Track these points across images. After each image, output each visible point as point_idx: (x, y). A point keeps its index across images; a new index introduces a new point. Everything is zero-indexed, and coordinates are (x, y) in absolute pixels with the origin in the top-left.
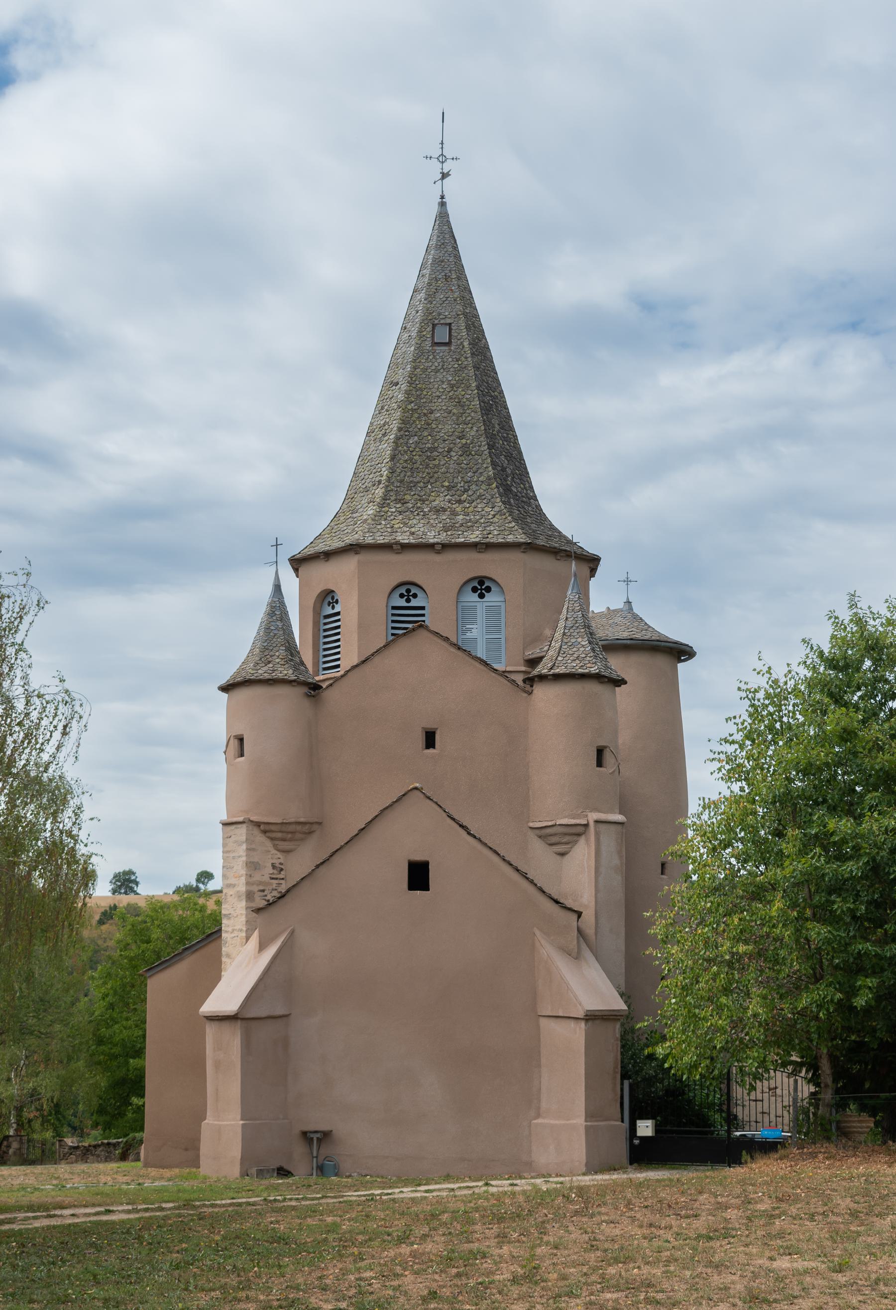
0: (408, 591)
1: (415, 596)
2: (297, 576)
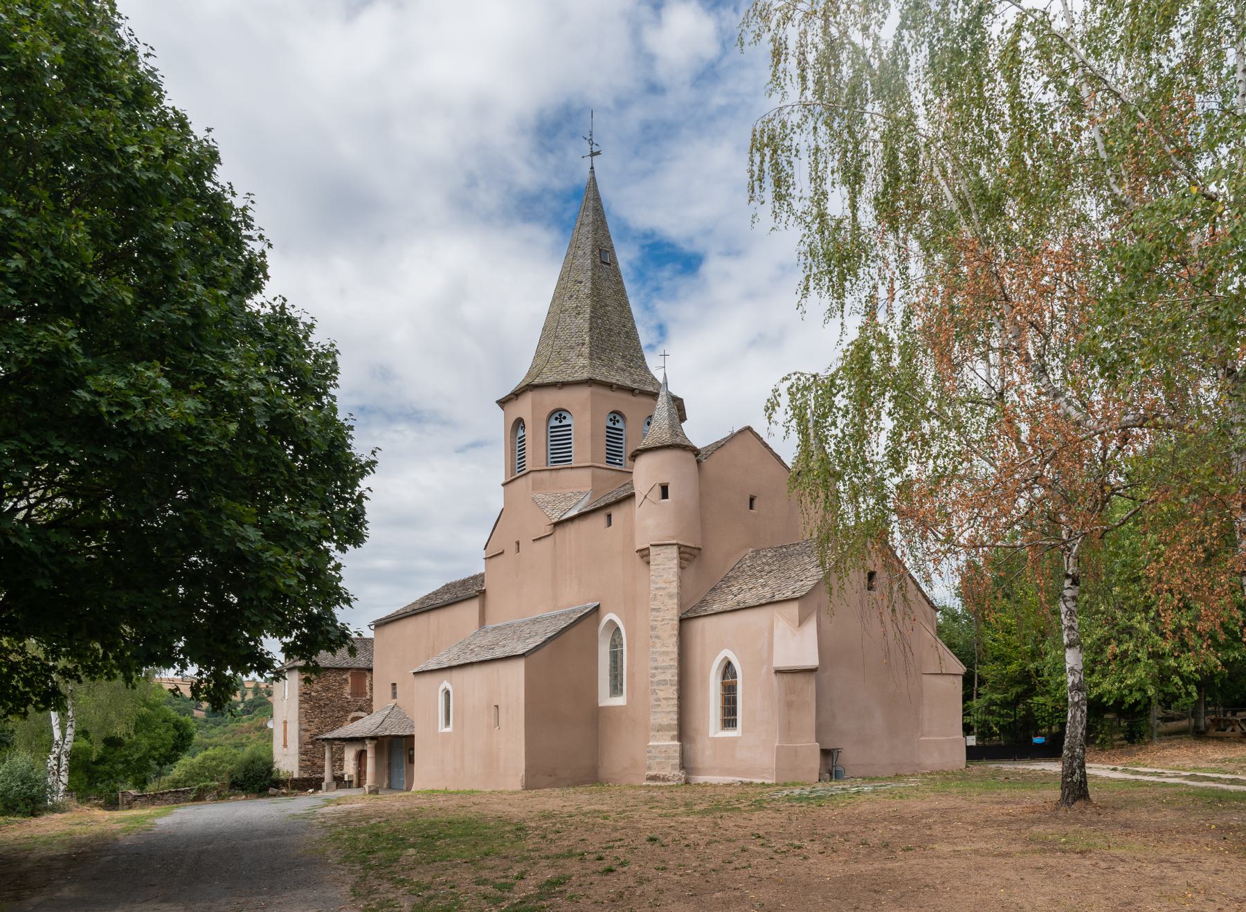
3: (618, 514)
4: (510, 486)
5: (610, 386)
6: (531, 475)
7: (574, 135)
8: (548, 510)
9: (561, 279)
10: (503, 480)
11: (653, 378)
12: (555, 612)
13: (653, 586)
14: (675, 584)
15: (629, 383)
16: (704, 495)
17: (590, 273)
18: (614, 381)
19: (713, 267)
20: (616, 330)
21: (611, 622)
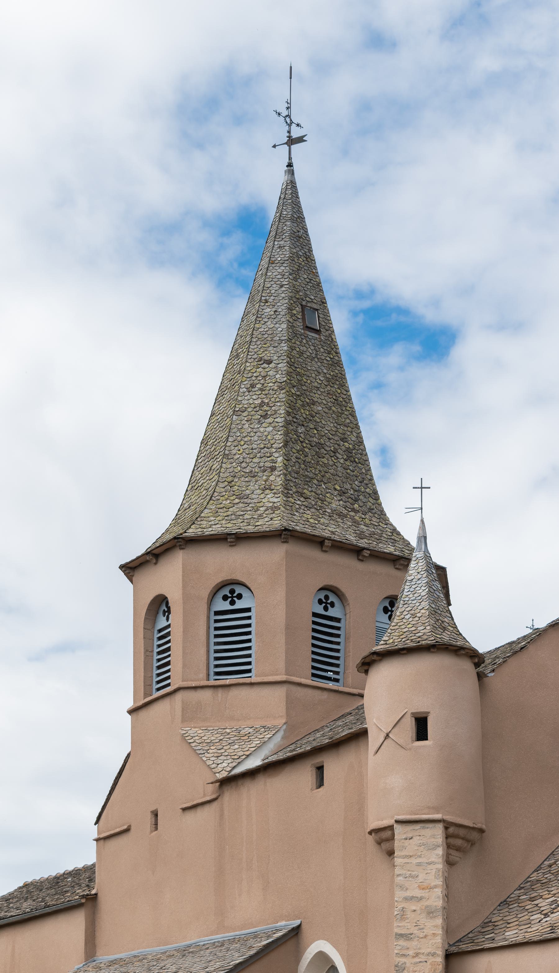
0: (232, 591)
1: (240, 596)
2: (132, 583)
3: (336, 766)
4: (143, 714)
5: (319, 542)
6: (179, 697)
7: (239, 120)
8: (210, 758)
9: (234, 355)
10: (130, 704)
11: (394, 531)
12: (219, 937)
13: (399, 894)
14: (439, 892)
15: (352, 538)
16: (489, 737)
17: (285, 347)
18: (326, 534)
19: (473, 349)
20: (330, 446)
21: (322, 956)
